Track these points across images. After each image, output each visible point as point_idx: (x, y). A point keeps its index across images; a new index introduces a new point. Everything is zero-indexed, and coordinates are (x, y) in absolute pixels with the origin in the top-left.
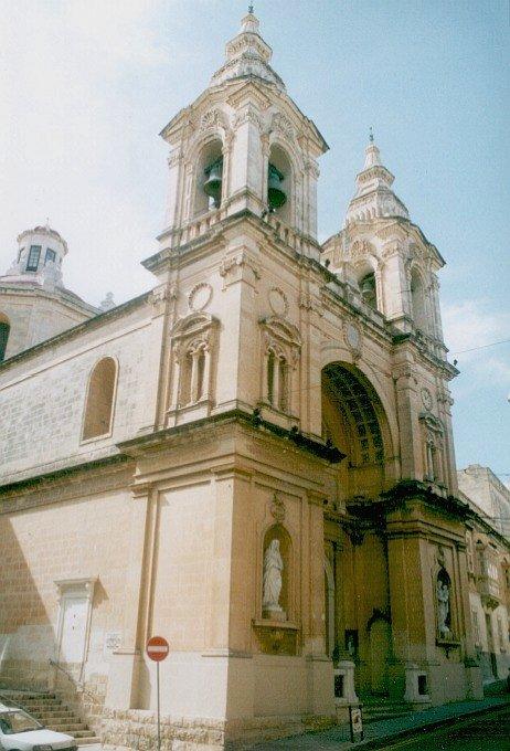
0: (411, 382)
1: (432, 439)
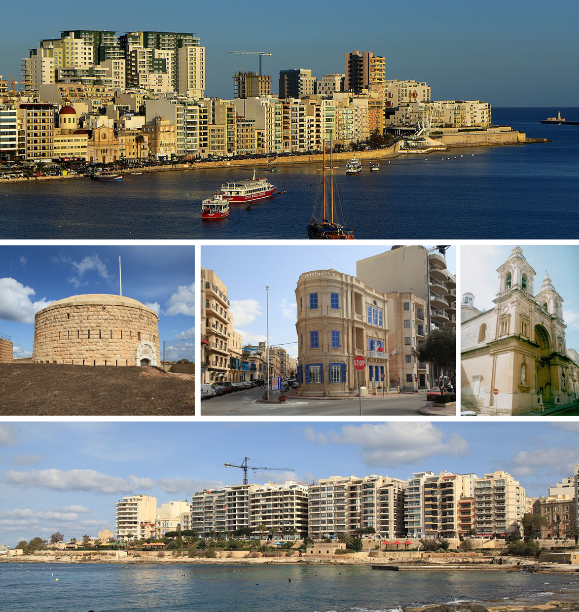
0: (556, 329)
1: (561, 342)
